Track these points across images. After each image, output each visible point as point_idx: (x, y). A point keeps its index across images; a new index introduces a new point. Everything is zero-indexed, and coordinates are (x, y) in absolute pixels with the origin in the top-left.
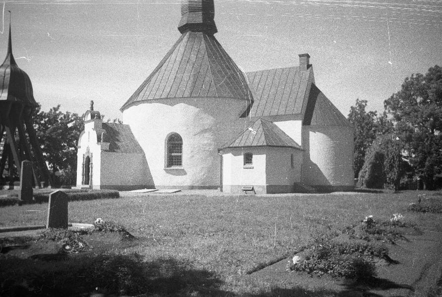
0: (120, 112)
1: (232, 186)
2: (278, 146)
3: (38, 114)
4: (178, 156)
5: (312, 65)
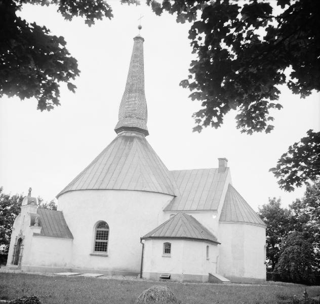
0: (56, 198)
1: (151, 273)
2: (105, 177)
3: (206, 100)
4: (104, 243)
5: (229, 168)
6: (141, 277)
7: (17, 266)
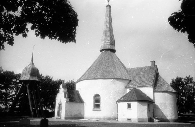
4: (99, 104)
6: (117, 120)
7: (59, 117)
